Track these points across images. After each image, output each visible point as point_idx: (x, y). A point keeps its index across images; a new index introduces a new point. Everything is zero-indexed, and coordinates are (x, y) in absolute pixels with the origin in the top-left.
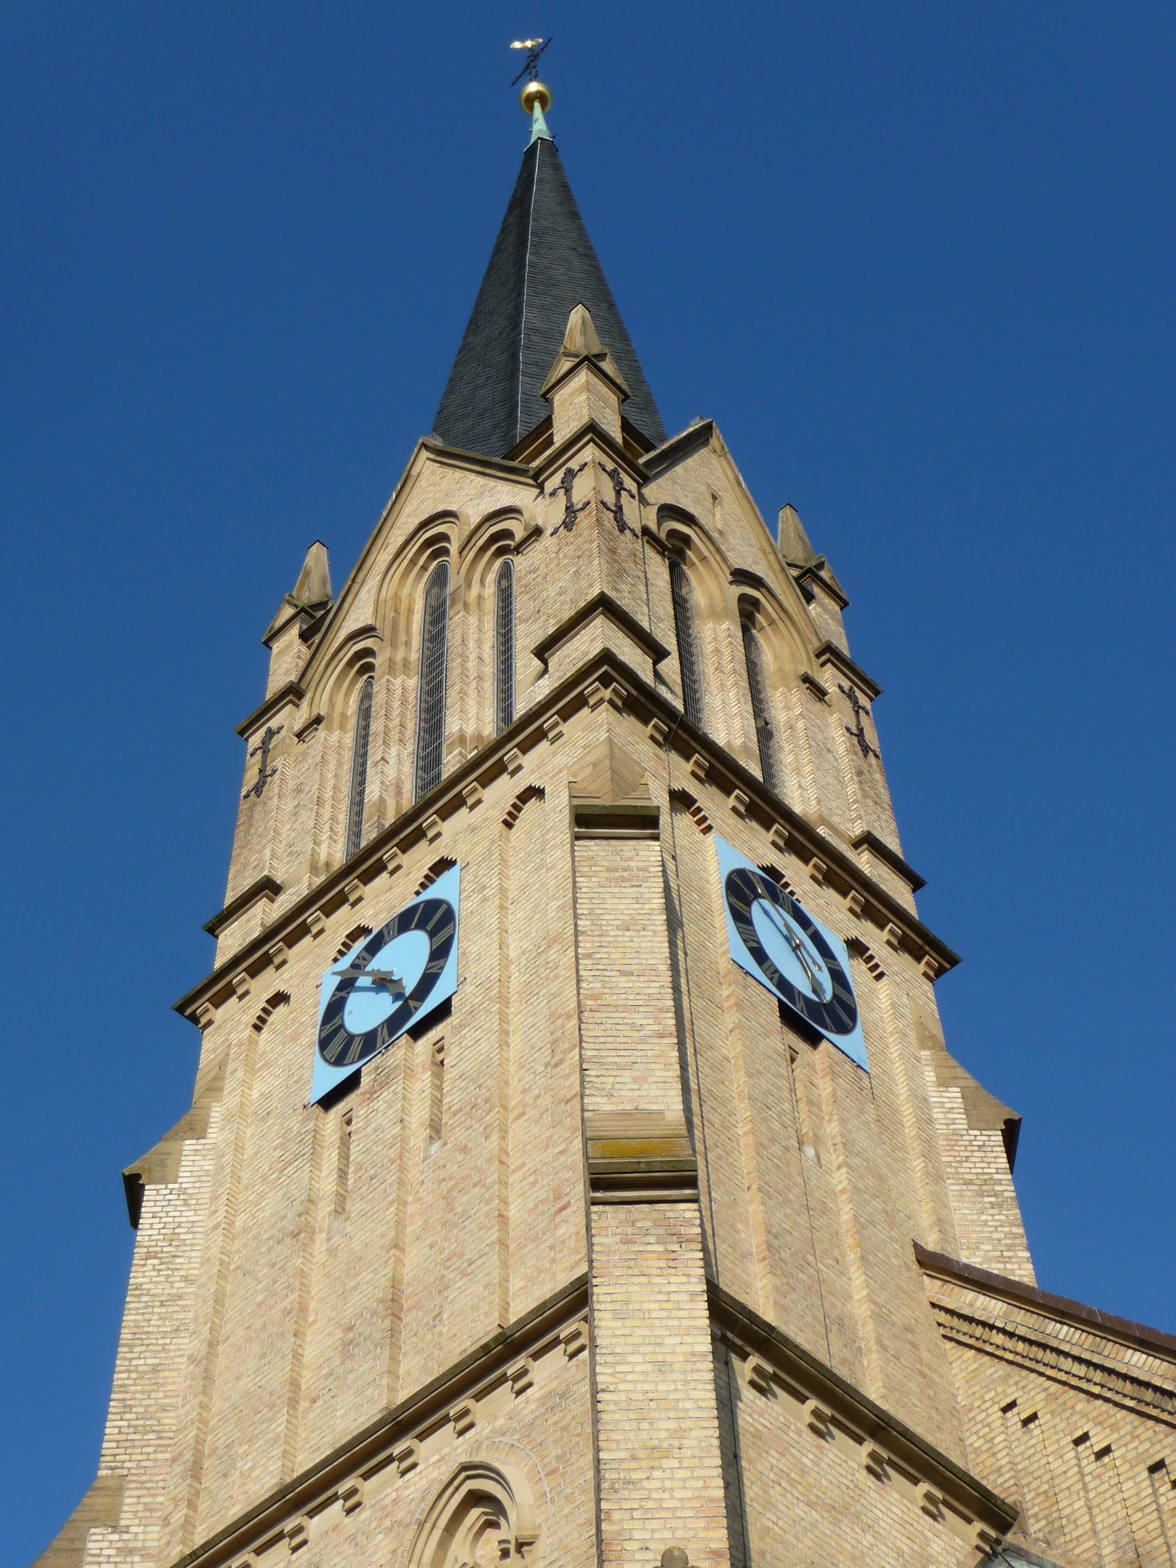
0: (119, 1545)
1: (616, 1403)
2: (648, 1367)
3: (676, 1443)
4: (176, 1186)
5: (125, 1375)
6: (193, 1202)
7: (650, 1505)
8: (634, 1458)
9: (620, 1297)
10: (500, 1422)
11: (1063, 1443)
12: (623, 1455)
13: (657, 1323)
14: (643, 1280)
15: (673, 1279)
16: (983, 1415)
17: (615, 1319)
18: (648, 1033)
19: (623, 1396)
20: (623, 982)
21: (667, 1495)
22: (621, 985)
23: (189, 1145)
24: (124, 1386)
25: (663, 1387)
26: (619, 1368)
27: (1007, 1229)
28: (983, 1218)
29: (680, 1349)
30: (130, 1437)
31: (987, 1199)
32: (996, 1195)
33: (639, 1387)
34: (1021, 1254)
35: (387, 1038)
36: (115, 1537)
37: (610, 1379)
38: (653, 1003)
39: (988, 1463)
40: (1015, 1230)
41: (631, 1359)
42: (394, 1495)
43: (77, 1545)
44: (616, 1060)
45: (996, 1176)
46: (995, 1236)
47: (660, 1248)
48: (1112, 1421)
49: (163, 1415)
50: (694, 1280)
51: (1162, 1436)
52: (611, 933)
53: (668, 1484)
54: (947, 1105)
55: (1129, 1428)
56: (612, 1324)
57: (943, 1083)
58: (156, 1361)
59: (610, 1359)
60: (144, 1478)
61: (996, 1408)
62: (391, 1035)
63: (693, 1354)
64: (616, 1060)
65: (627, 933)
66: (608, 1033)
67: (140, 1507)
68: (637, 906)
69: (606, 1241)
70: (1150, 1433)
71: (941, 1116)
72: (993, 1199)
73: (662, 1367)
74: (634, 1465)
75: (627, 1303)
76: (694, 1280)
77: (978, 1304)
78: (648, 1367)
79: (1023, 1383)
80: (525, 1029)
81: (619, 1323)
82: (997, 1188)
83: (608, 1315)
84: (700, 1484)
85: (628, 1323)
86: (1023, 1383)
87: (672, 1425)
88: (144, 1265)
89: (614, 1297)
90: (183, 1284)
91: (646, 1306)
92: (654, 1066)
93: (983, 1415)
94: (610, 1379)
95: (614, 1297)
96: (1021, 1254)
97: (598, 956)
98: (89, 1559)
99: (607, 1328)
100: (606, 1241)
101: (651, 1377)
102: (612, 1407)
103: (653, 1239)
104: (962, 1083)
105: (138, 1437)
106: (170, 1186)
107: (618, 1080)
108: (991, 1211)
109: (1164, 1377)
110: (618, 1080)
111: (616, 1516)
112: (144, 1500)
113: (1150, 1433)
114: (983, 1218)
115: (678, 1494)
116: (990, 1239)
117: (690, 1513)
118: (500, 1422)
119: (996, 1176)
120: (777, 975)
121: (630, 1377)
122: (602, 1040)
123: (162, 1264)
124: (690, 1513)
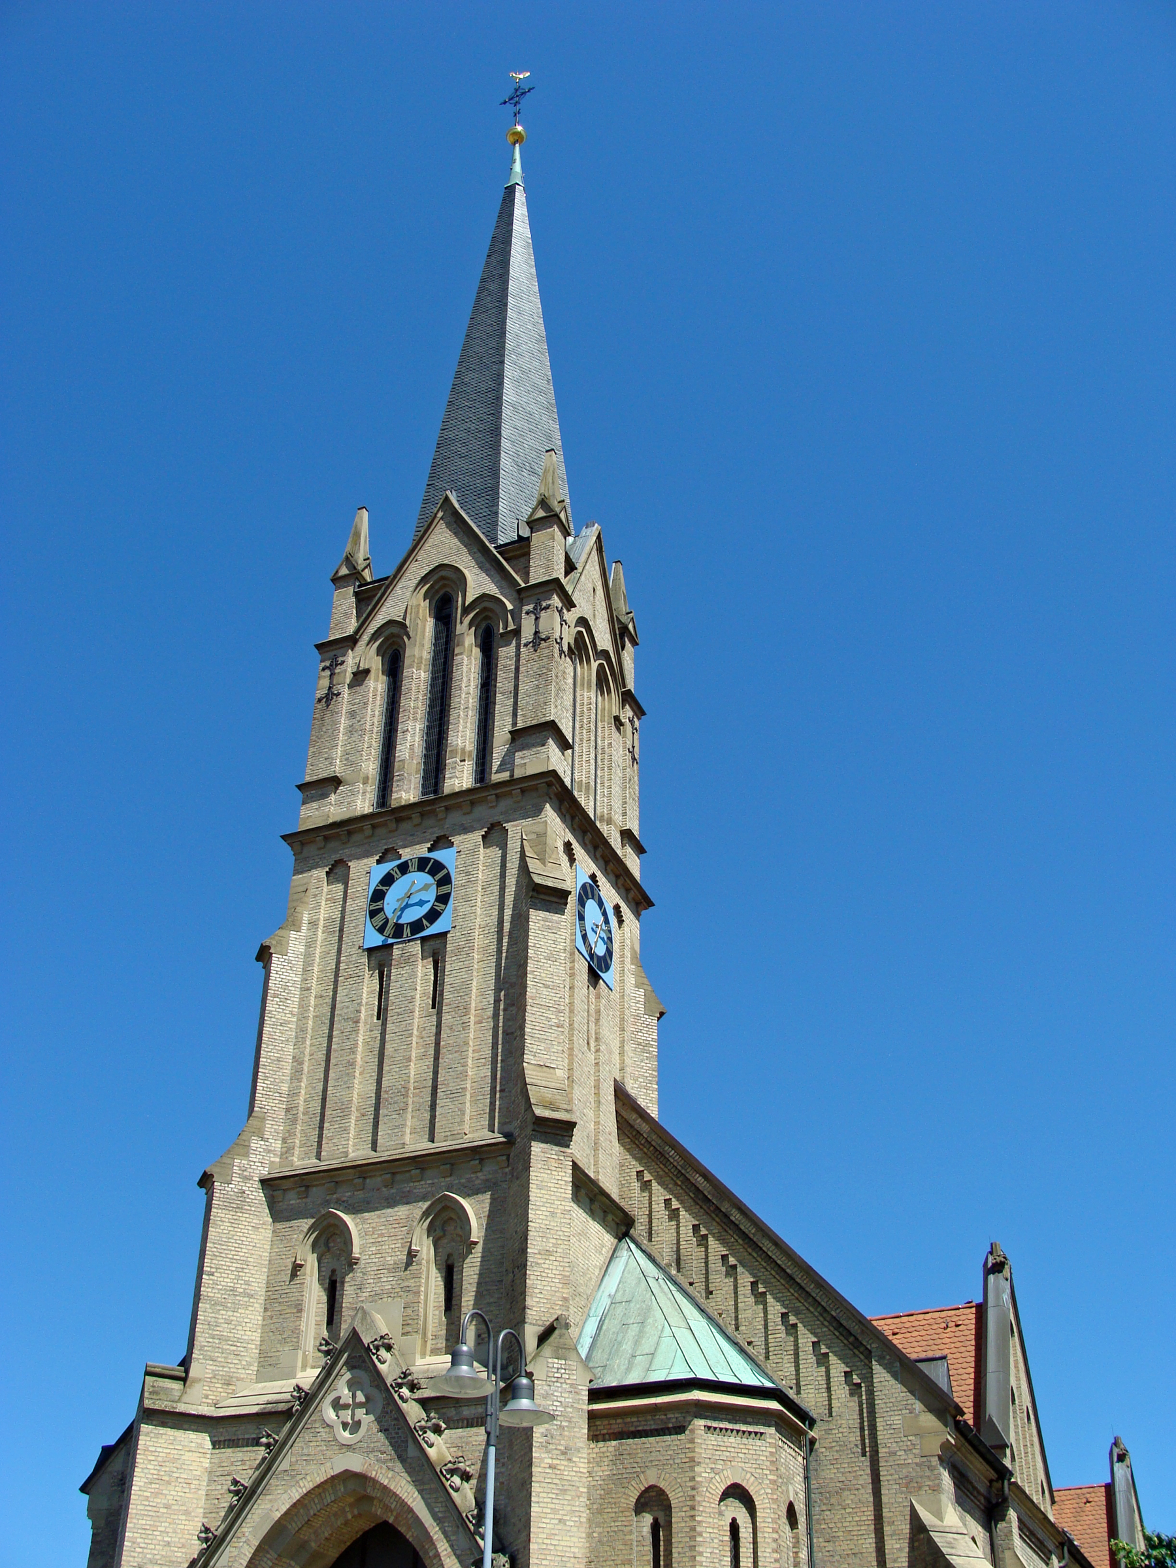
0: (264, 1147)
1: (535, 1228)
2: (548, 1214)
3: (555, 1250)
4: (287, 957)
5: (265, 1060)
6: (295, 969)
7: (544, 1274)
8: (540, 1254)
9: (540, 1179)
10: (463, 1181)
11: (660, 1198)
12: (536, 1251)
13: (552, 1193)
14: (549, 1172)
15: (560, 1174)
16: (628, 1170)
17: (537, 1188)
18: (553, 1024)
19: (538, 1225)
20: (545, 992)
21: (550, 1272)
22: (544, 993)
23: (293, 934)
24: (264, 1065)
25: (552, 1224)
26: (537, 1212)
27: (650, 1072)
28: (642, 1064)
29: (560, 1207)
30: (268, 1093)
31: (645, 1055)
32: (649, 1053)
33: (544, 1222)
34: (654, 1086)
35: (409, 935)
36: (262, 1143)
37: (533, 1216)
38: (556, 1006)
39: (626, 1193)
40: (654, 1073)
41: (542, 1208)
42: (408, 1189)
43: (247, 1144)
44: (539, 1036)
45: (651, 1043)
46: (646, 1075)
47: (556, 1157)
48: (682, 1198)
49: (282, 1085)
50: (568, 1175)
51: (701, 1214)
52: (542, 961)
53: (551, 1267)
54: (637, 999)
55: (688, 1204)
56: (536, 1191)
57: (638, 986)
58: (279, 1055)
59: (534, 1207)
60: (275, 1116)
61: (635, 1170)
62: (412, 935)
63: (565, 1210)
64: (539, 1036)
65: (549, 962)
66: (537, 1020)
67: (273, 1130)
68: (554, 946)
69: (536, 1150)
70: (697, 1211)
71: (634, 1004)
72: (648, 1055)
73: (553, 1214)
74: (539, 1256)
75: (542, 1181)
76: (568, 1175)
77: (638, 1121)
78: (548, 1214)
79: (648, 1164)
80: (485, 973)
81: (539, 1191)
82: (651, 1049)
83: (534, 1186)
84: (562, 1269)
85: (543, 1192)
86: (648, 1164)
87: (554, 1241)
88: (272, 1001)
89: (538, 1178)
90: (290, 1016)
91: (549, 1185)
92: (554, 1043)
93: (628, 1170)
94: (533, 1216)
95: (538, 1178)
96: (654, 1086)
97: (535, 973)
98: (252, 1151)
99: (534, 1192)
100: (536, 1150)
101: (549, 1218)
102: (533, 1229)
103: (554, 1153)
104: (645, 987)
105: (271, 1094)
106: (284, 957)
107: (539, 1047)
108: (646, 1061)
109: (709, 1192)
110: (539, 1047)
111: (532, 1277)
112: (274, 1127)
113: (697, 1211)
114: (642, 1064)
115: (554, 1272)
116: (643, 1076)
117: (558, 1281)
118: (463, 1181)
119: (651, 1043)
120: (584, 932)
121: (541, 1217)
122: (534, 1023)
123: (281, 1002)
124: (558, 1281)
